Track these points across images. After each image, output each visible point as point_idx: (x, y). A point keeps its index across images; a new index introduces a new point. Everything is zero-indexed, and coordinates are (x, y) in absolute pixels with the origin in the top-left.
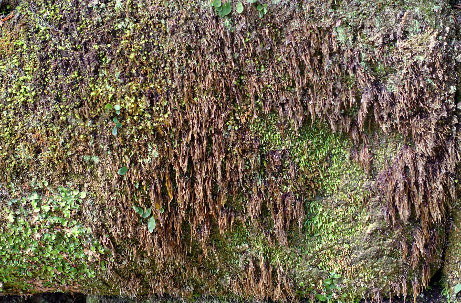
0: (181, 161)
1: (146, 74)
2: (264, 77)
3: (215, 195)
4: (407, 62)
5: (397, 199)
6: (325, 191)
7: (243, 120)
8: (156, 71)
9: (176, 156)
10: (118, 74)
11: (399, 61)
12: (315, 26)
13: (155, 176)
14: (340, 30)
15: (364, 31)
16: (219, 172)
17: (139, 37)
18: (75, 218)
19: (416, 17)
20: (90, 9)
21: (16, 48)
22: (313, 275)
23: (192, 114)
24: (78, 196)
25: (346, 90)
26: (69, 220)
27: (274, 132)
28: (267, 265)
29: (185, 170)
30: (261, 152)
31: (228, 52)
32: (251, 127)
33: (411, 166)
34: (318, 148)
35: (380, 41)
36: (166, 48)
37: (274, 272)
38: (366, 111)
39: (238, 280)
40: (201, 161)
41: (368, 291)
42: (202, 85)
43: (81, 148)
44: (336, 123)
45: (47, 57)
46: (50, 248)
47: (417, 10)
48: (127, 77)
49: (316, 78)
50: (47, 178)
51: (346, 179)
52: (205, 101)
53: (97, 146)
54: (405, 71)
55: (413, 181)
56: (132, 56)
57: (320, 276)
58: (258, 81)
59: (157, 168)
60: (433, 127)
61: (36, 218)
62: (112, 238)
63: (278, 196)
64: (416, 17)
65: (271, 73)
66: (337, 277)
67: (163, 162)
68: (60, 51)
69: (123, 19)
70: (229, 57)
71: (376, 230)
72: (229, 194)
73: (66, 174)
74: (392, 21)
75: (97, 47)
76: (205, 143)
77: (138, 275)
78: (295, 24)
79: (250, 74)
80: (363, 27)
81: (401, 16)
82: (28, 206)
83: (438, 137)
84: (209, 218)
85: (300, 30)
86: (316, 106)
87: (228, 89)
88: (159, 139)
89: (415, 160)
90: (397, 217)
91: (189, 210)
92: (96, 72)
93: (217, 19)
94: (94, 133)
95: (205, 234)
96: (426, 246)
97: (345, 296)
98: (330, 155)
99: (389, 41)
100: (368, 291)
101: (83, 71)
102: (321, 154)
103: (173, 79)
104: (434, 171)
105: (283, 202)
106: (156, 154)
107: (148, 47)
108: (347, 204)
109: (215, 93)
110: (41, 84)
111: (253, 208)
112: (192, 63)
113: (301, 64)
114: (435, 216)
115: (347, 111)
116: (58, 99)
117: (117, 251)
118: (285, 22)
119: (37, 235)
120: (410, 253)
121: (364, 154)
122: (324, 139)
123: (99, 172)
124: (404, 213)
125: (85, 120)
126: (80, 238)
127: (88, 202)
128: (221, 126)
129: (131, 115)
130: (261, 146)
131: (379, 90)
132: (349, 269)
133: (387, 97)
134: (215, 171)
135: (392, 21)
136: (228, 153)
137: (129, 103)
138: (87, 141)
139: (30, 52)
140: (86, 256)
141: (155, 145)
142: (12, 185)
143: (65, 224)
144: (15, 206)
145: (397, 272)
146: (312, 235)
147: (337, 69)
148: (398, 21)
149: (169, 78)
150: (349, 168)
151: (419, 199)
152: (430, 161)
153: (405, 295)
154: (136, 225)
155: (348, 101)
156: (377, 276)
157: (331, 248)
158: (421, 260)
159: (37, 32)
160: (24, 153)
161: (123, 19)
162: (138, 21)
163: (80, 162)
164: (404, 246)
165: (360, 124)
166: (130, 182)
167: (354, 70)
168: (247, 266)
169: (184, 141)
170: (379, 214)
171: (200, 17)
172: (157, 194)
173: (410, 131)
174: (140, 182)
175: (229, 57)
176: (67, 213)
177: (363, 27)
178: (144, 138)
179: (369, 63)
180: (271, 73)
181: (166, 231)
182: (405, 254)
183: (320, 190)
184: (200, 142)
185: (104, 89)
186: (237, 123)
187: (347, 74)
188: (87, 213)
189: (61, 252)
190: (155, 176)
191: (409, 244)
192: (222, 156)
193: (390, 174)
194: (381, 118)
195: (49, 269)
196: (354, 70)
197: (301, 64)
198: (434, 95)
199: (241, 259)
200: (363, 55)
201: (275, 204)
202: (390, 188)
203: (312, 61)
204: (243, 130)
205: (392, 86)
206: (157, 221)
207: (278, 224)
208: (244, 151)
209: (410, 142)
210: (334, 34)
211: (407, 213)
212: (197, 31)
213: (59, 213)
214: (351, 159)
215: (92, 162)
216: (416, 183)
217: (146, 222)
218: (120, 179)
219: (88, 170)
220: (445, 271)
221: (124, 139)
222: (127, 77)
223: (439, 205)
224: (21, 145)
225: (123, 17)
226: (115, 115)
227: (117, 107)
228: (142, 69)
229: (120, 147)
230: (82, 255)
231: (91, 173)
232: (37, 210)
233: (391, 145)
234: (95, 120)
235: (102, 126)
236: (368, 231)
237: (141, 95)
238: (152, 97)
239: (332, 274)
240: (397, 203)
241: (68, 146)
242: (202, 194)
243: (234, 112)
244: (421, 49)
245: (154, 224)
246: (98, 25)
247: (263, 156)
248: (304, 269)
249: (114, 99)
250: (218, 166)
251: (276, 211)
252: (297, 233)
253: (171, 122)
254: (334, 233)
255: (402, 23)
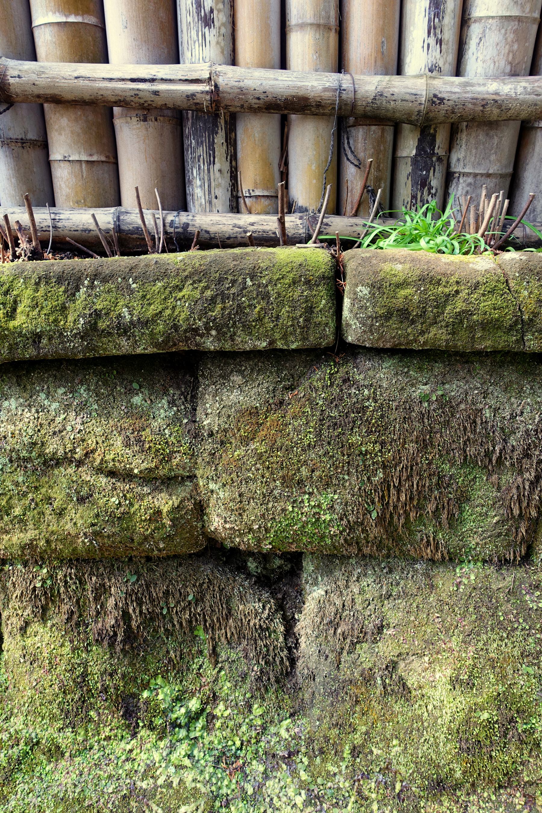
0: (395, 480)
1: (379, 431)
2: (444, 434)
3: (411, 499)
4: (522, 428)
5: (512, 504)
6: (470, 498)
7: (430, 458)
8: (385, 430)
9: (392, 476)
10: (364, 431)
11: (518, 428)
12: (474, 408)
13: (379, 488)
14: (487, 411)
15: (500, 411)
16: (415, 486)
17: (377, 411)
18: (328, 509)
19: (528, 404)
20: (350, 394)
21: (304, 412)
22: (460, 546)
23: (404, 453)
24: (332, 497)
25: (488, 442)
26: (324, 510)
27: (446, 464)
28: (434, 539)
29: (397, 485)
30: (439, 475)
31: (426, 421)
32: (434, 461)
33: (521, 486)
34: (469, 474)
35: (509, 417)
36: (392, 418)
37: (438, 543)
38: (498, 455)
39: (414, 547)
40: (405, 481)
41: (490, 556)
42: (410, 439)
43: (340, 471)
44: (481, 461)
45: (324, 420)
46: (310, 526)
47: (529, 400)
48: (369, 432)
49: (472, 436)
50: (316, 486)
51: (483, 491)
52: (412, 447)
53: (349, 470)
54: (521, 433)
55: (522, 494)
56: (373, 421)
57: (464, 546)
58: (441, 436)
59: (381, 483)
60: (535, 464)
61: (306, 509)
62: (349, 521)
63: (445, 500)
64: (528, 404)
65: (448, 432)
66: (473, 547)
67: (384, 480)
68: (331, 416)
69: (368, 401)
70: (427, 423)
71: (499, 521)
72: (418, 499)
73: (327, 485)
74: (515, 406)
75: (353, 415)
76: (409, 470)
77: (357, 543)
78: (463, 406)
79: (436, 433)
80: (499, 408)
81: (520, 403)
82: (302, 501)
83: (537, 470)
84: (405, 512)
85: (465, 410)
86: (471, 451)
87: (424, 440)
88: (384, 467)
89: (523, 483)
90: (512, 514)
91: (395, 507)
92: (352, 429)
93: (421, 402)
94: (348, 463)
95: (402, 520)
96: (526, 531)
97: (476, 558)
98: (475, 477)
99: (513, 417)
100: (490, 556)
101: (344, 428)
102: (471, 477)
103: (394, 435)
104: (534, 488)
105: (448, 504)
106: (381, 475)
107: (382, 416)
108: (483, 506)
109: (417, 443)
110: (319, 434)
111: (431, 507)
112: (406, 426)
113: (465, 428)
114: (533, 513)
115: (488, 454)
116: (329, 443)
117: (350, 529)
118: (457, 405)
119: (304, 519)
120: (517, 535)
121: (494, 477)
122: (473, 468)
123: (347, 484)
124: (516, 512)
125: (344, 455)
126: (330, 521)
127: (339, 501)
128: (419, 461)
129: (371, 454)
130: (439, 472)
131: (506, 443)
132: (481, 542)
133: (510, 447)
134: (413, 485)
135: (515, 406)
136: (420, 475)
137: (370, 447)
138: (343, 466)
139: (313, 416)
140: (330, 531)
141: (381, 470)
142: (294, 490)
143: (322, 513)
144: (294, 502)
145: (509, 545)
146: (461, 522)
147: (484, 431)
148: (518, 406)
149: (392, 433)
150: (485, 485)
151: (525, 504)
152: (532, 483)
153: (512, 558)
154: (364, 514)
155: (488, 449)
156: (497, 547)
157: (471, 530)
158: (523, 538)
159: (317, 404)
160: (304, 472)
161: (368, 401)
162: (376, 402)
163: (337, 478)
164: (514, 531)
165: (494, 462)
166: (365, 490)
167: (494, 432)
168: (422, 540)
169: (398, 469)
170: (501, 512)
171: (412, 401)
172: (379, 497)
173: (521, 466)
174: (371, 490)
175: (427, 423)
176: (324, 507)
177: (499, 408)
178: (376, 466)
179: (502, 429)
180: (448, 432)
181: (381, 519)
182: (514, 535)
183: (468, 497)
184: (407, 470)
185: (355, 439)
186: (427, 459)
187: (489, 434)
188: (337, 507)
189: (315, 529)
190: (379, 488)
191: (517, 529)
192: (418, 478)
193: (509, 489)
194: (506, 458)
195: (304, 538)
196: (494, 432)
197: (465, 428)
198: (536, 447)
199: (419, 535)
200: (499, 424)
201: (443, 505)
202: (509, 498)
203: (471, 426)
204: (430, 464)
205: (512, 441)
206: (378, 513)
207: (444, 516)
208: (430, 475)
209: (521, 472)
210: (484, 412)
211: (518, 512)
212: (410, 408)
213: (319, 506)
214: (487, 480)
215: (344, 479)
216: (524, 495)
217: (370, 512)
218: (360, 489)
219: (341, 482)
220: (534, 545)
221: (365, 466)
222: (369, 432)
223: (535, 508)
224: (304, 468)
225: (368, 400)
226: (361, 453)
227: (363, 449)
228: (379, 429)
229: (362, 471)
230: (327, 531)
231: (343, 485)
232: (307, 504)
233: (509, 473)
234: (349, 456)
235: (353, 459)
236: (494, 521)
237: (376, 443)
238: (383, 444)
239: (471, 545)
240: (512, 506)
241: (332, 469)
242: (404, 498)
243: (426, 453)
244: (530, 422)
245: (376, 514)
246: (354, 403)
247: (439, 478)
248: (455, 541)
249: (361, 444)
250: (415, 483)
251: (444, 508)
252: (454, 522)
253: (392, 458)
254: (474, 522)
255: (520, 408)
